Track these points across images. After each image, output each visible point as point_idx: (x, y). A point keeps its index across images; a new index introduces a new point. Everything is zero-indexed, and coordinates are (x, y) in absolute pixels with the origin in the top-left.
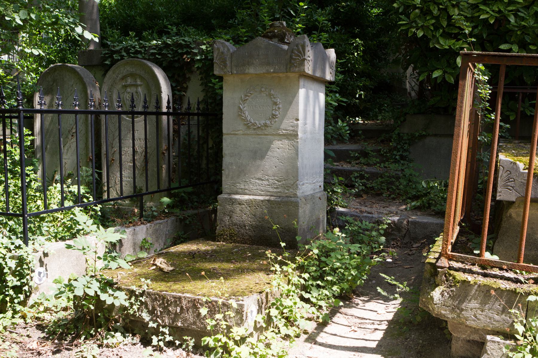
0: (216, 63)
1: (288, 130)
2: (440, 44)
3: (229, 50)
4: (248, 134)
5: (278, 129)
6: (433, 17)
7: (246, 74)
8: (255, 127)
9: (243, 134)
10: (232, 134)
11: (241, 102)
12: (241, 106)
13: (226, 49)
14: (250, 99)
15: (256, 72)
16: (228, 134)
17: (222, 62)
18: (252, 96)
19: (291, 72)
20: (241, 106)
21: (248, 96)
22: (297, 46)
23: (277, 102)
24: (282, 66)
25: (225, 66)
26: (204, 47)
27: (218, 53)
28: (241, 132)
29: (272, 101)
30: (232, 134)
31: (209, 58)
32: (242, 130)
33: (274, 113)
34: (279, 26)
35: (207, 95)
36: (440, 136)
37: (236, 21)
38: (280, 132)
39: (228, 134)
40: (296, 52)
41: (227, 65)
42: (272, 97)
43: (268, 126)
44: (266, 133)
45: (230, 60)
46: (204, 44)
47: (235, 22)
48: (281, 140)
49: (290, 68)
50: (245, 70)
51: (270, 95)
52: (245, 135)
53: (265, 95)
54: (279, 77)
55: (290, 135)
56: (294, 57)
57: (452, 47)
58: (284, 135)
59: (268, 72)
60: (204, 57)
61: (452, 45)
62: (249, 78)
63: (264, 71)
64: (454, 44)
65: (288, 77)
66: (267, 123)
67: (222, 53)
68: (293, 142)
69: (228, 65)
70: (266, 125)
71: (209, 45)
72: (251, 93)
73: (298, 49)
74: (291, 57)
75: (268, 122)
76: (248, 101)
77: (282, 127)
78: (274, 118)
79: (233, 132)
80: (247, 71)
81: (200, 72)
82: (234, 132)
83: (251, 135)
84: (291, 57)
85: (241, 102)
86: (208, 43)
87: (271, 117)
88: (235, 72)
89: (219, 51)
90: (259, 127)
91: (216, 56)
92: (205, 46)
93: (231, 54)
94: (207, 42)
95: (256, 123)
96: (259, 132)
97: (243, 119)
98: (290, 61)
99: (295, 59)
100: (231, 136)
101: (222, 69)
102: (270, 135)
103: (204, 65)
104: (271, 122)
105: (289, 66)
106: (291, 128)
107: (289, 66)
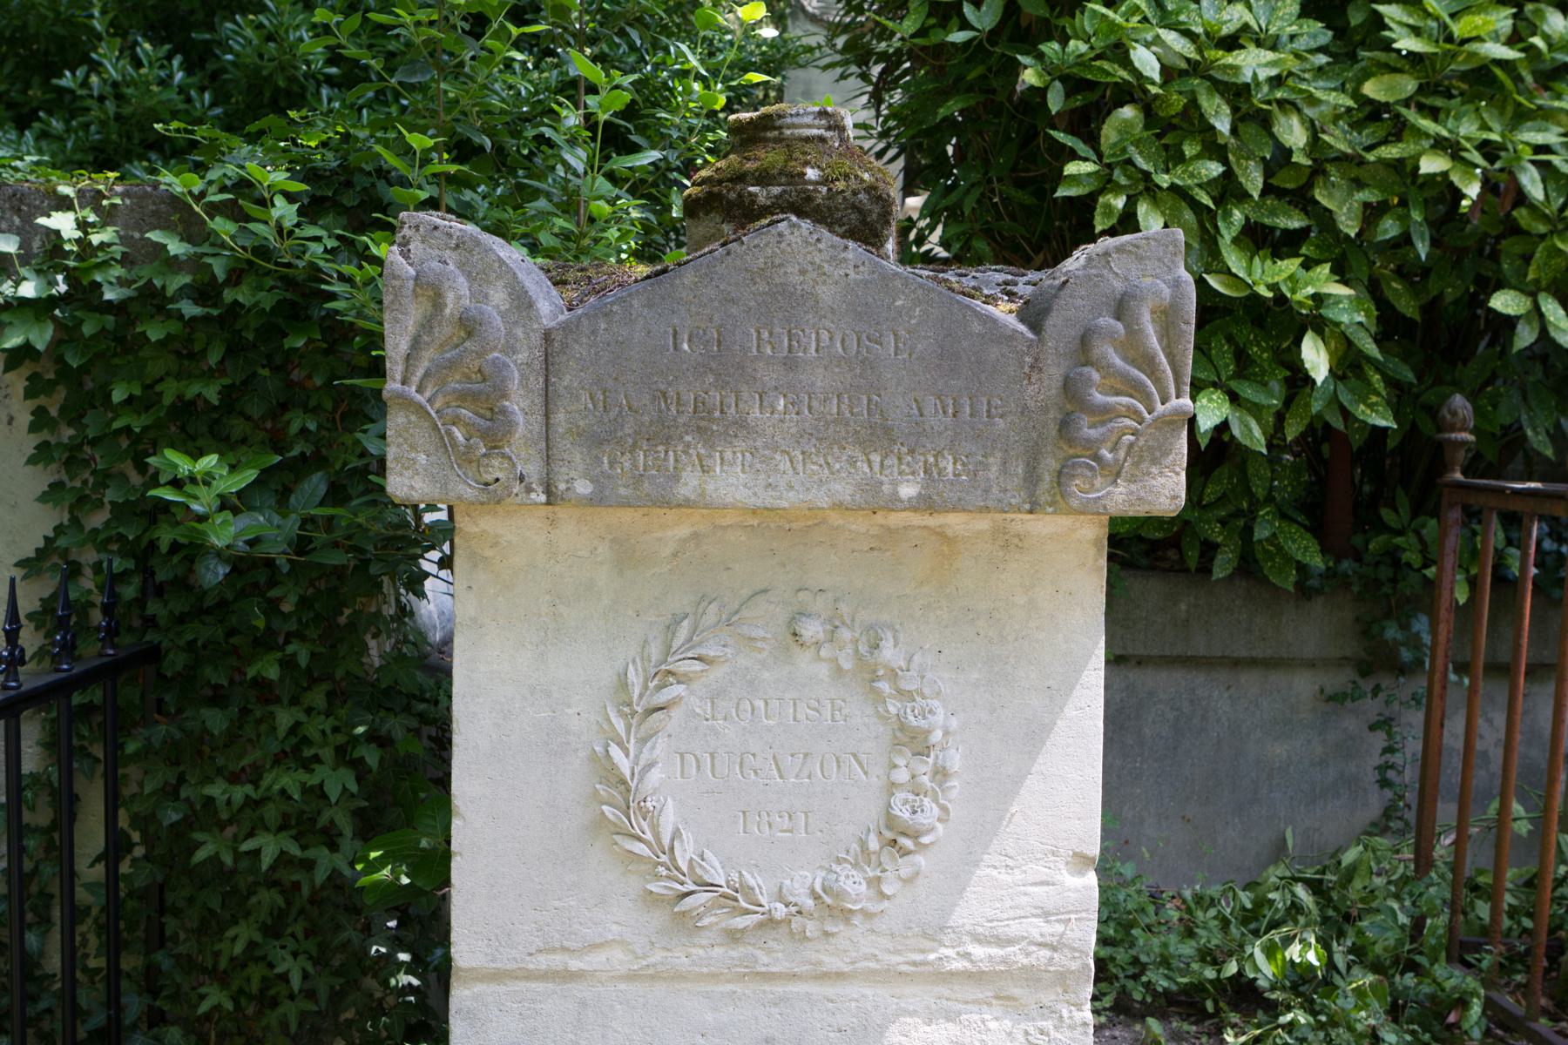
0: (408, 404)
1: (1010, 942)
2: (1229, 272)
3: (522, 303)
4: (678, 977)
5: (934, 933)
6: (1214, 149)
7: (687, 504)
8: (741, 922)
9: (632, 977)
10: (530, 976)
11: (620, 726)
12: (615, 752)
13: (498, 296)
14: (694, 703)
15: (766, 498)
16: (497, 976)
17: (463, 397)
18: (717, 673)
19: (1071, 511)
20: (615, 752)
21: (682, 679)
22: (1122, 308)
23: (928, 732)
24: (994, 462)
25: (494, 429)
26: (63, 223)
27: (427, 325)
28: (617, 958)
29: (884, 718)
30: (530, 976)
31: (109, 295)
32: (622, 943)
33: (904, 814)
34: (822, 139)
35: (75, 521)
36: (1139, 663)
37: (94, 79)
38: (948, 956)
39: (497, 976)
40: (1118, 362)
41: (510, 425)
42: (884, 686)
43: (846, 915)
44: (833, 963)
45: (537, 383)
46: (64, 204)
47: (85, 83)
48: (951, 1017)
49: (1061, 477)
50: (676, 478)
51: (869, 674)
52: (652, 977)
53: (823, 670)
54: (941, 535)
55: (1031, 976)
56: (1099, 398)
57: (1284, 289)
58: (975, 977)
59: (876, 501)
60: (63, 288)
61: (1285, 281)
62: (684, 531)
63: (843, 490)
64: (1291, 278)
65: (1009, 543)
66: (848, 886)
67: (469, 326)
68: (1048, 1025)
69: (521, 430)
70: (832, 906)
71: (97, 209)
72: (710, 651)
73: (1134, 333)
74: (1071, 390)
75: (853, 883)
76: (676, 713)
77: (962, 917)
78: (906, 853)
79: (543, 962)
80: (690, 483)
81: (33, 378)
82: (557, 961)
83: (700, 977)
84: (1071, 390)
85: (620, 726)
86: (93, 199)
87: (874, 844)
88: (583, 487)
89: (437, 302)
90: (770, 923)
91: (404, 346)
92: (70, 216)
93: (547, 336)
94: (80, 193)
95: (747, 891)
96: (774, 956)
97: (639, 858)
98: (1065, 425)
99: (1105, 414)
100: (521, 986)
101: (466, 457)
102: (871, 976)
103: (67, 335)
104: (874, 883)
105: (1050, 464)
106: (1037, 928)
107: (1050, 464)
